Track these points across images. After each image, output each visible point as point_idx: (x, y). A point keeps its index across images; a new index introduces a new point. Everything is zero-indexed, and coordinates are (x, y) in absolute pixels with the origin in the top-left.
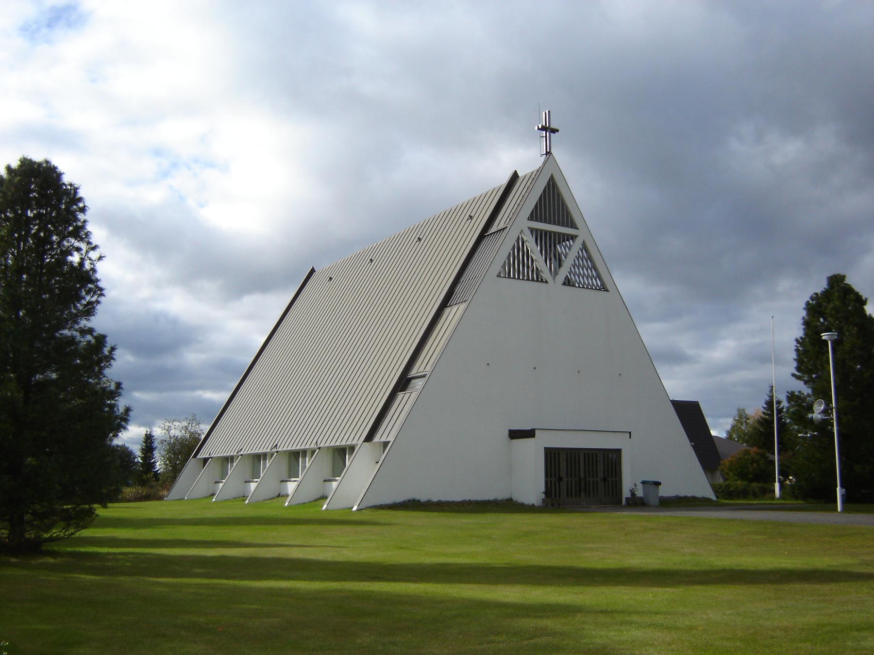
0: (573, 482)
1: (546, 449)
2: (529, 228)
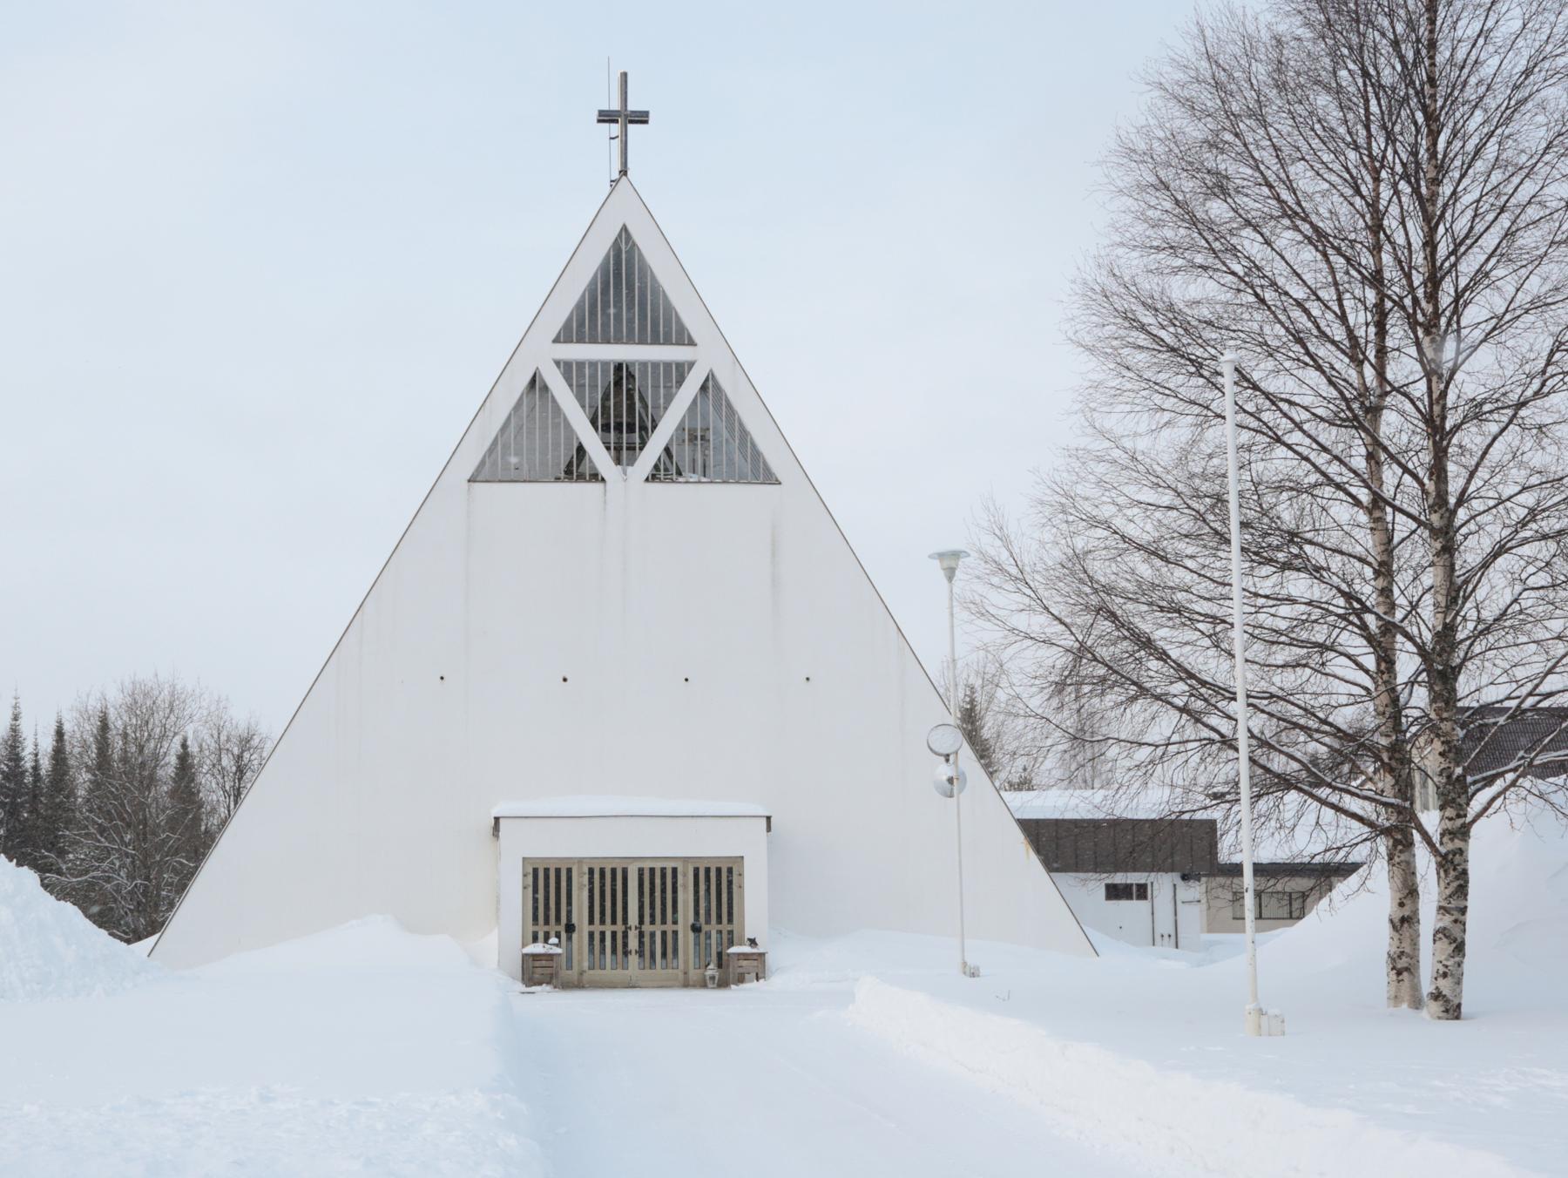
2: (557, 363)
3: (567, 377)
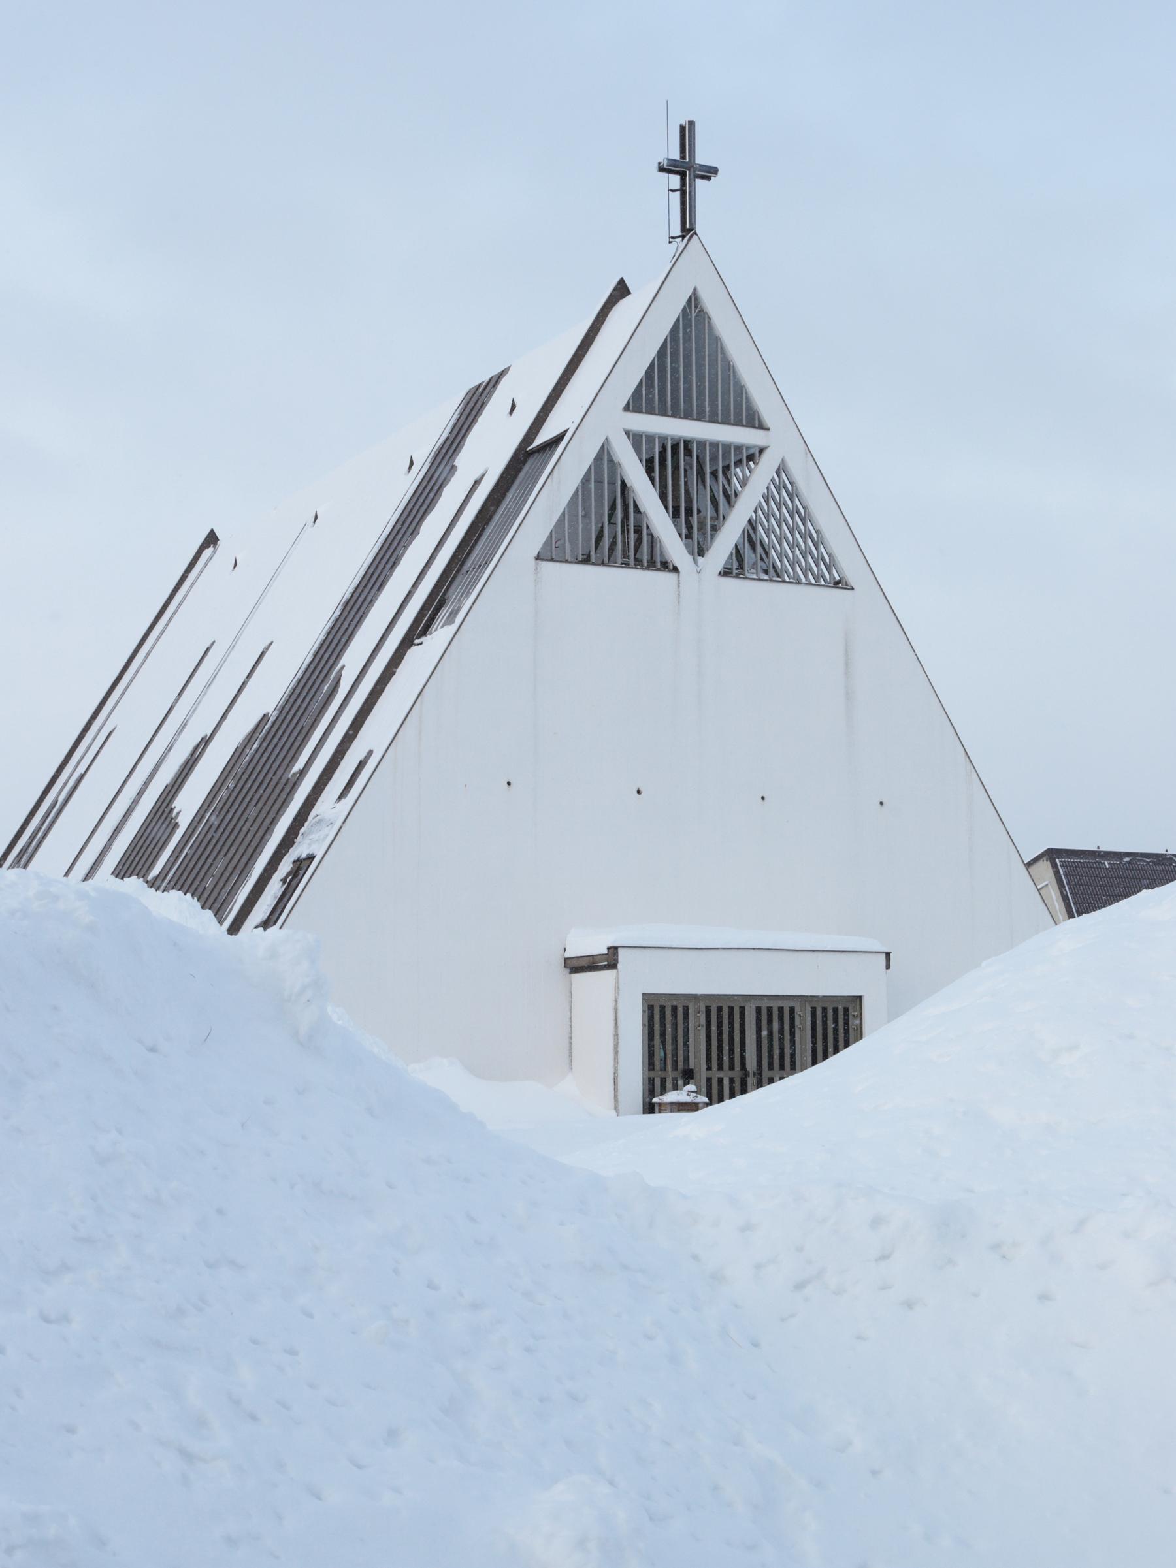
0: (726, 1082)
1: (646, 997)
2: (627, 433)
3: (637, 447)
